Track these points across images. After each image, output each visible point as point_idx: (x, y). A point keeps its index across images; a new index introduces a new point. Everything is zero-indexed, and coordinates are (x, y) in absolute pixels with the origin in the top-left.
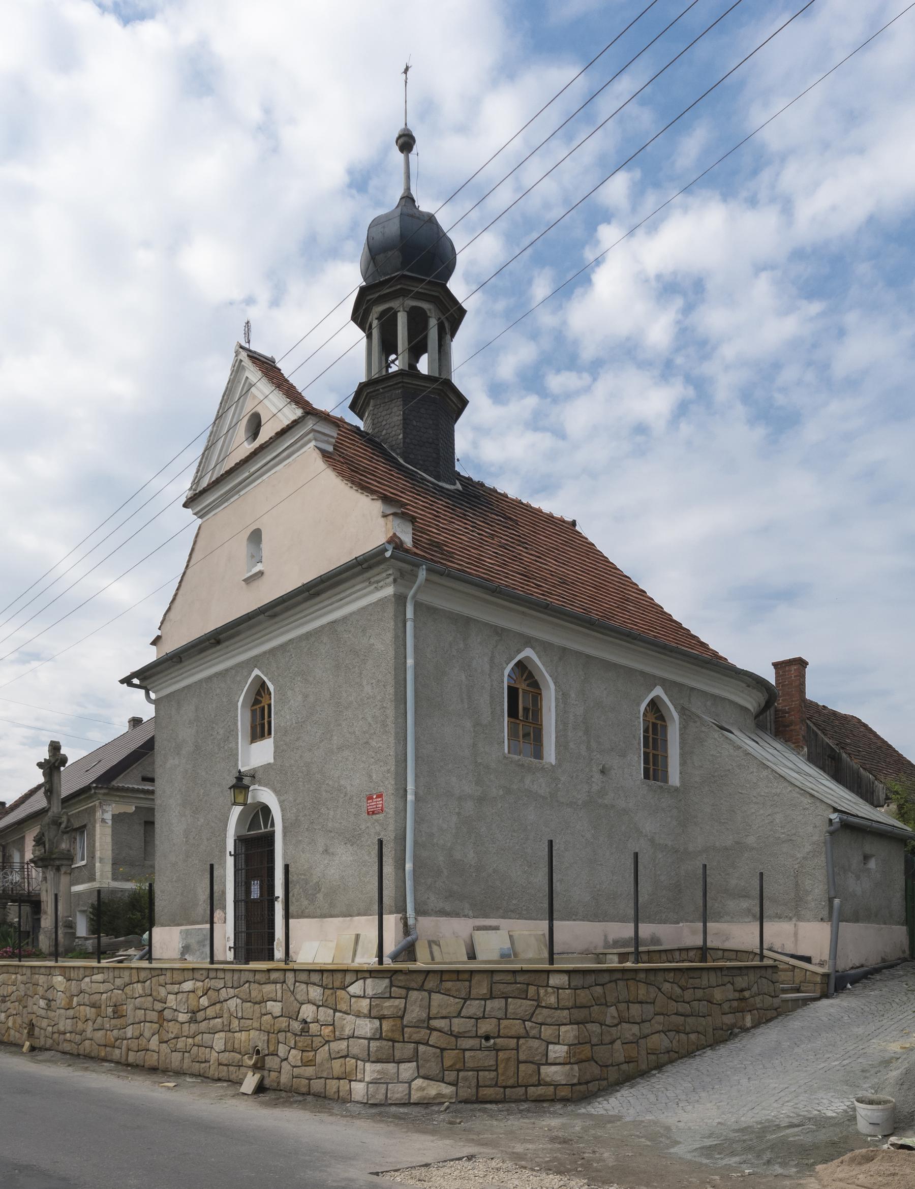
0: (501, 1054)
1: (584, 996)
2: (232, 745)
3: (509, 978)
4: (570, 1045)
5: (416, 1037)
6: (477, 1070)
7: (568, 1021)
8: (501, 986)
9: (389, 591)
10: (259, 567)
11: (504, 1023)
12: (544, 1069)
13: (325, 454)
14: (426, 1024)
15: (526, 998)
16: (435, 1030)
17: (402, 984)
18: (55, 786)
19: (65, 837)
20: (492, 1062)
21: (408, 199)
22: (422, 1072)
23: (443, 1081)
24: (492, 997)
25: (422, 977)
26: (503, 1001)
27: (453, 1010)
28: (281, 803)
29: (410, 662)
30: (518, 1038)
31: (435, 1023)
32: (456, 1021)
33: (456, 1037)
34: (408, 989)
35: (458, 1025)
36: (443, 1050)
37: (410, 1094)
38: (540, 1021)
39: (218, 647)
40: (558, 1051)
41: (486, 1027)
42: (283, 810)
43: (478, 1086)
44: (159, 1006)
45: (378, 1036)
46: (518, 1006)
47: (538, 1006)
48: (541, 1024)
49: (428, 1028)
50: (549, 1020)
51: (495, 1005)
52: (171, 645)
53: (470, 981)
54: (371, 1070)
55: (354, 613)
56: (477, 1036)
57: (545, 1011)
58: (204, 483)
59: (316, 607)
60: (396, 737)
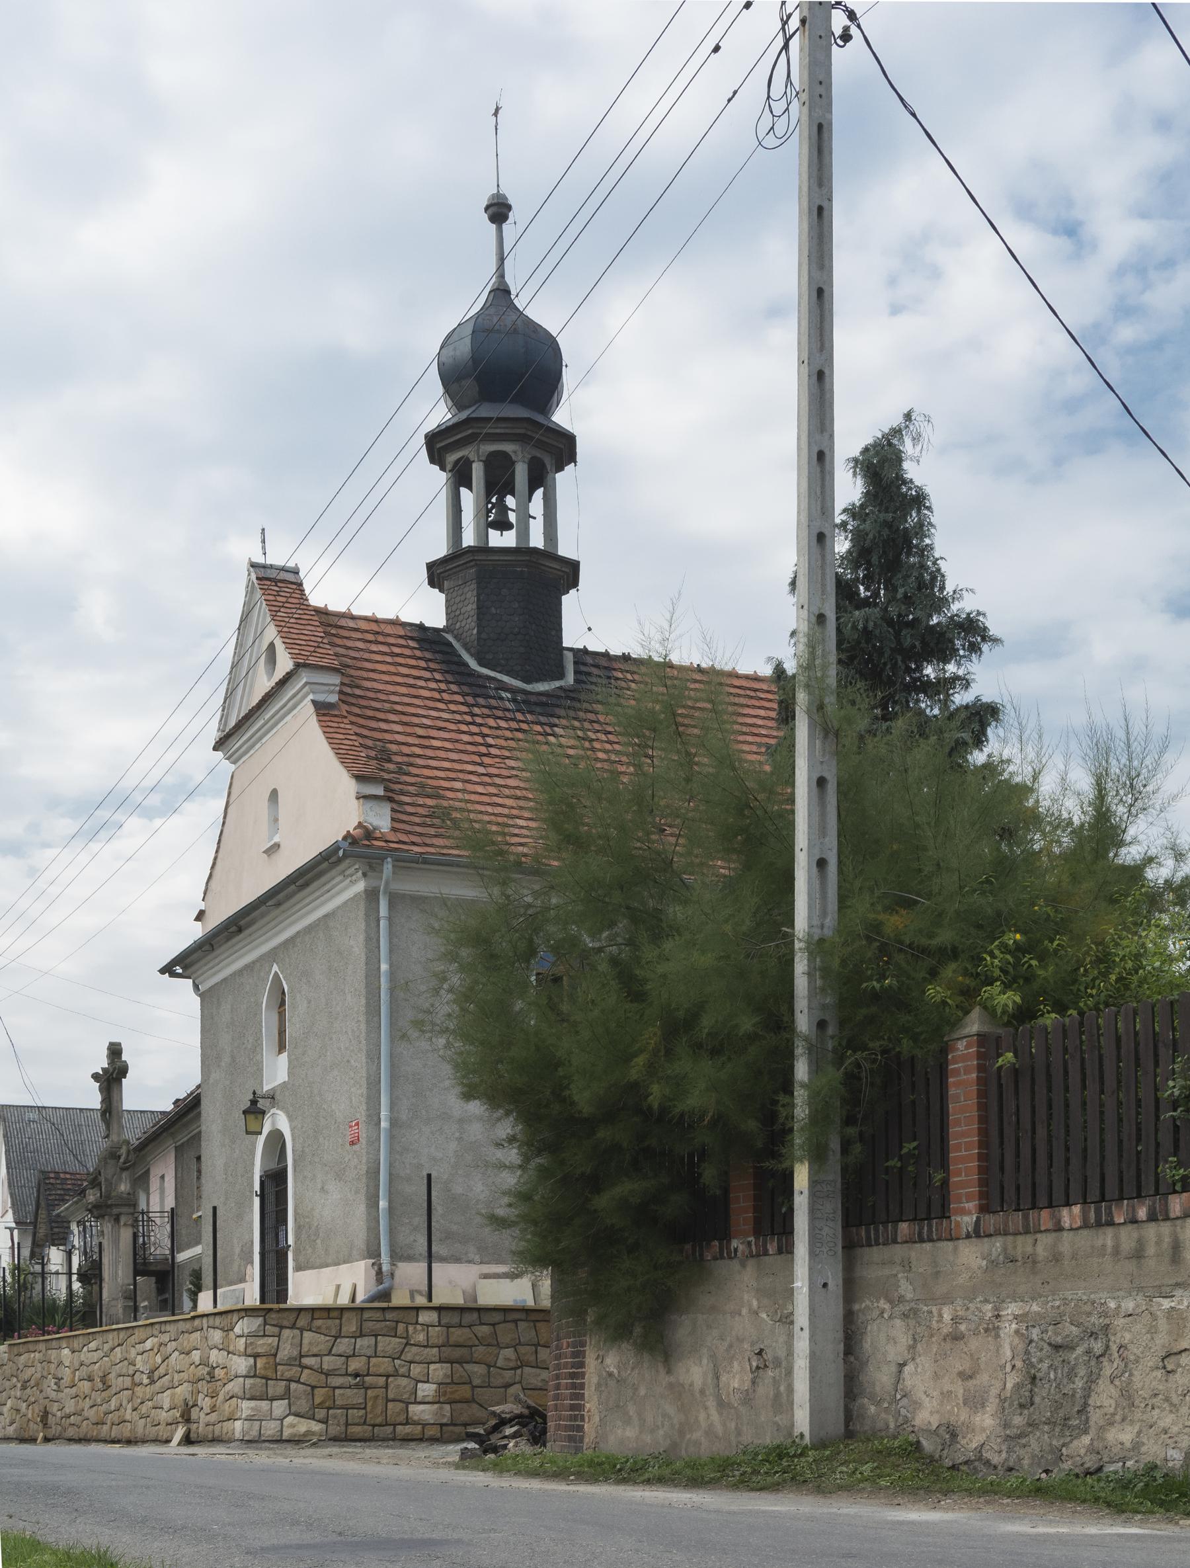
0: (369, 1392)
1: (458, 1335)
2: (258, 1057)
3: (378, 1315)
4: (439, 1384)
5: (287, 1375)
6: (346, 1408)
7: (437, 1359)
8: (371, 1324)
9: (360, 886)
10: (276, 839)
11: (373, 1360)
12: (412, 1408)
13: (321, 708)
14: (297, 1360)
15: (395, 1336)
16: (306, 1367)
17: (275, 1322)
18: (115, 1104)
19: (124, 1175)
20: (361, 1400)
21: (501, 293)
22: (293, 1409)
23: (313, 1419)
24: (361, 1336)
25: (294, 1315)
26: (373, 1338)
27: (323, 1348)
28: (292, 1129)
29: (384, 967)
30: (388, 1376)
31: (306, 1361)
32: (326, 1359)
33: (327, 1375)
34: (282, 1327)
35: (328, 1362)
36: (313, 1388)
37: (282, 1431)
38: (408, 1359)
39: (242, 936)
40: (426, 1390)
41: (355, 1365)
42: (293, 1140)
43: (347, 1424)
44: (131, 1370)
45: (252, 1374)
46: (388, 1344)
47: (407, 1344)
48: (411, 1362)
49: (300, 1365)
50: (417, 1358)
51: (364, 1343)
52: (215, 920)
53: (341, 1319)
54: (246, 1407)
55: (338, 908)
56: (347, 1374)
57: (414, 1349)
58: (232, 723)
59: (311, 898)
60: (368, 1056)
